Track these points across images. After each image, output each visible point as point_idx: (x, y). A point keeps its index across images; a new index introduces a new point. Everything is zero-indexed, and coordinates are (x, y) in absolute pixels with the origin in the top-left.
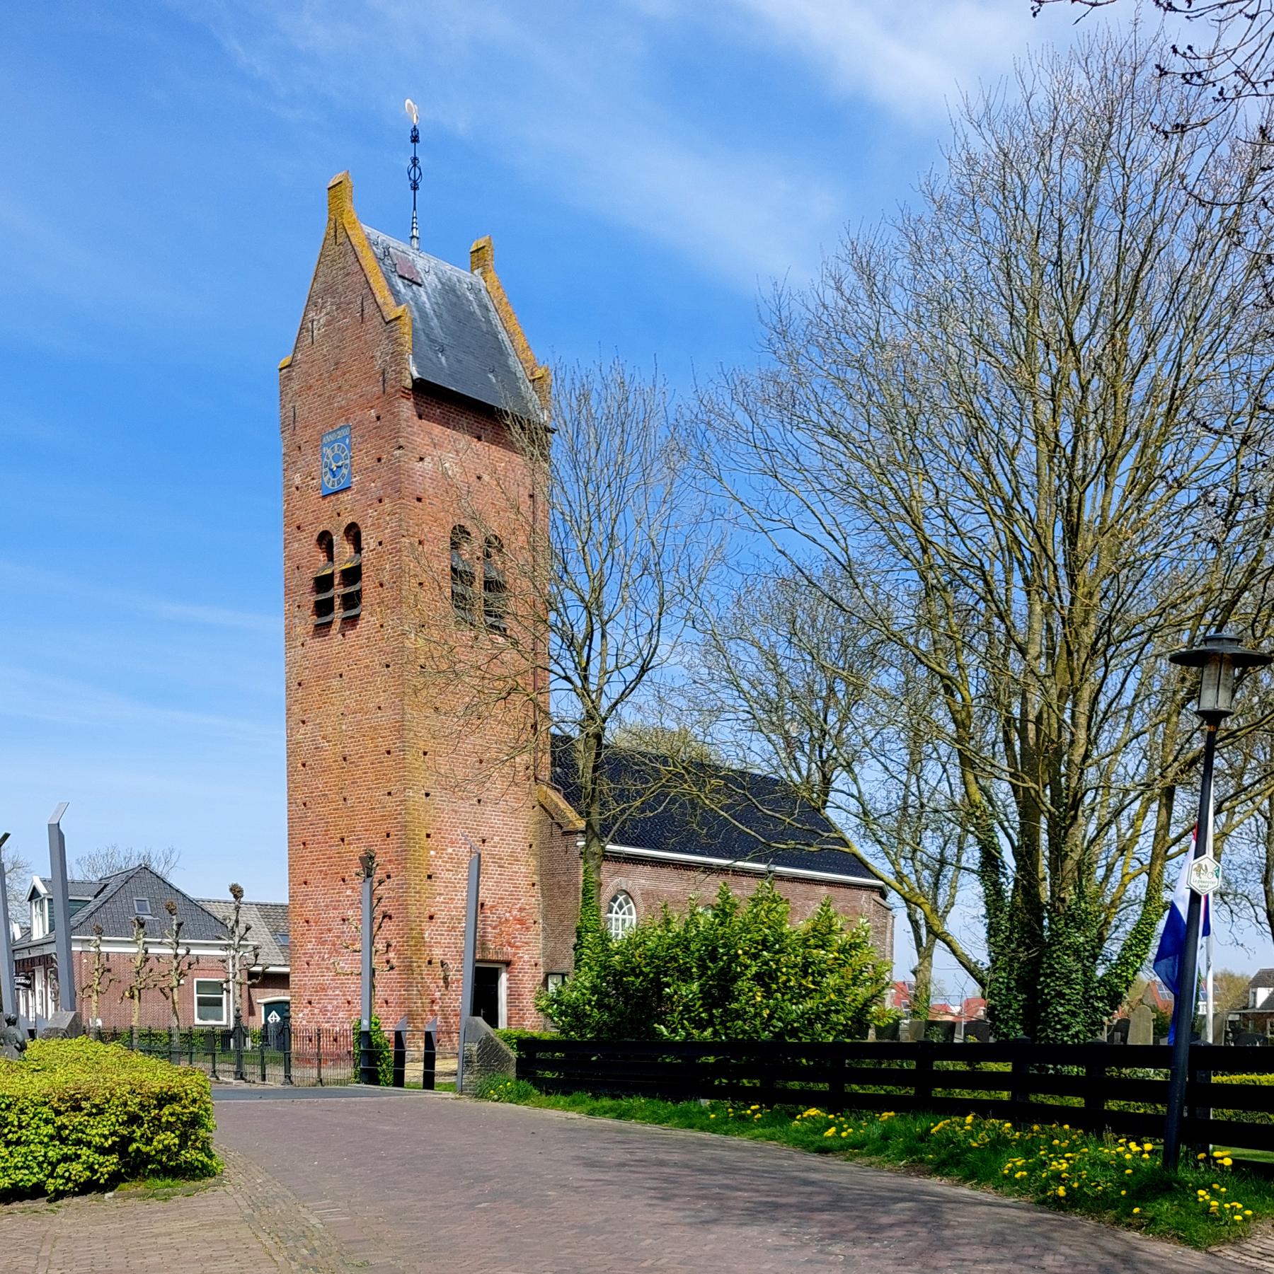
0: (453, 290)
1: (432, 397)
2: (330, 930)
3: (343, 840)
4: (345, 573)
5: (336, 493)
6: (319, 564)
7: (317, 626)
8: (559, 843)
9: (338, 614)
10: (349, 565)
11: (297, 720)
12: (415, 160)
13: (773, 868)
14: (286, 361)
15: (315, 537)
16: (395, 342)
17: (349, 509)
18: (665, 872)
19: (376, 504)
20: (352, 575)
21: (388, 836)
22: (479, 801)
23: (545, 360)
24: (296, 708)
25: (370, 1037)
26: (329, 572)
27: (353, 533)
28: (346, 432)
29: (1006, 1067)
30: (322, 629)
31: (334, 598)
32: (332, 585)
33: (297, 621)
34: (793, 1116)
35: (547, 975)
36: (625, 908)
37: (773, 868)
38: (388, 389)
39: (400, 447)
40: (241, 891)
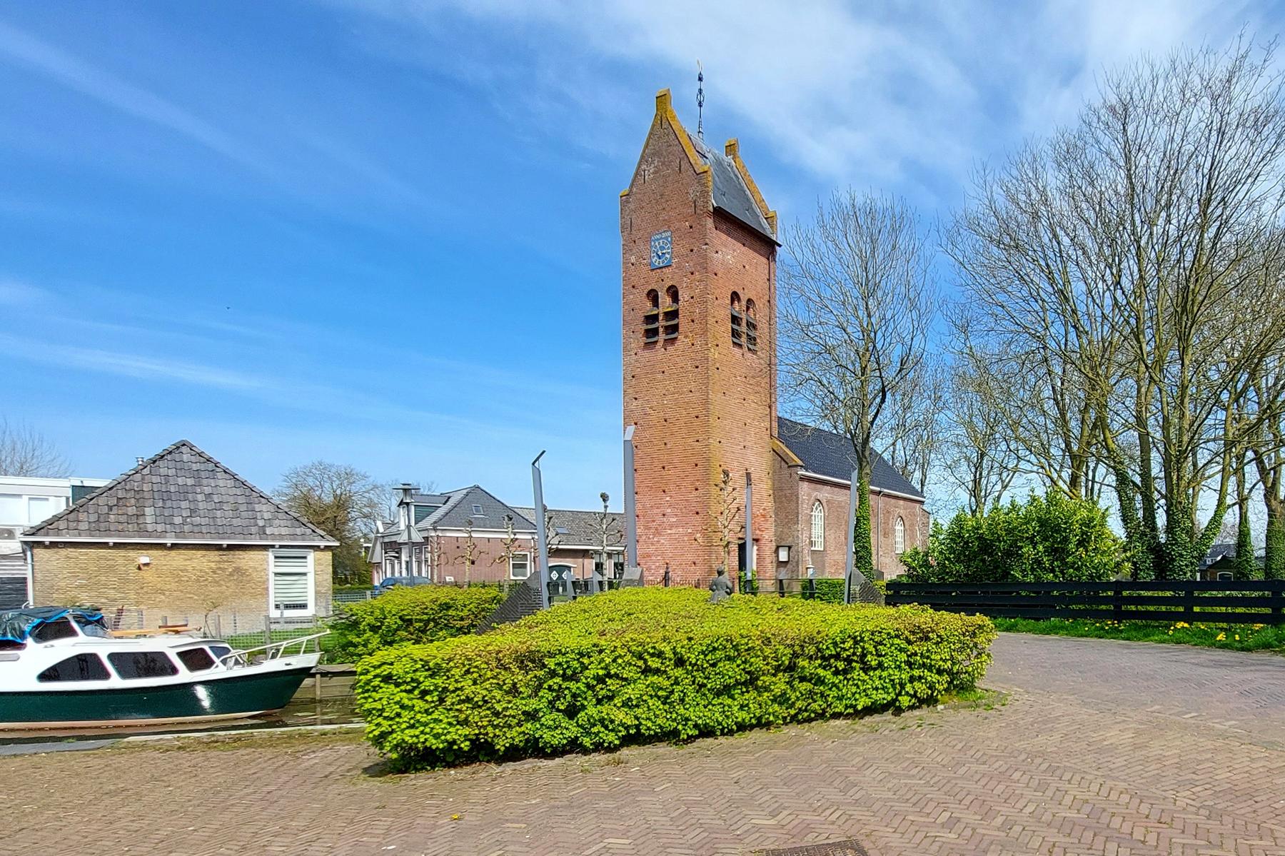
4: (666, 314)
6: (648, 308)
8: (786, 472)
9: (662, 336)
11: (631, 396)
12: (700, 91)
14: (626, 190)
20: (673, 315)
23: (778, 207)
24: (630, 391)
27: (674, 293)
31: (660, 325)
34: (1168, 628)
35: (778, 547)
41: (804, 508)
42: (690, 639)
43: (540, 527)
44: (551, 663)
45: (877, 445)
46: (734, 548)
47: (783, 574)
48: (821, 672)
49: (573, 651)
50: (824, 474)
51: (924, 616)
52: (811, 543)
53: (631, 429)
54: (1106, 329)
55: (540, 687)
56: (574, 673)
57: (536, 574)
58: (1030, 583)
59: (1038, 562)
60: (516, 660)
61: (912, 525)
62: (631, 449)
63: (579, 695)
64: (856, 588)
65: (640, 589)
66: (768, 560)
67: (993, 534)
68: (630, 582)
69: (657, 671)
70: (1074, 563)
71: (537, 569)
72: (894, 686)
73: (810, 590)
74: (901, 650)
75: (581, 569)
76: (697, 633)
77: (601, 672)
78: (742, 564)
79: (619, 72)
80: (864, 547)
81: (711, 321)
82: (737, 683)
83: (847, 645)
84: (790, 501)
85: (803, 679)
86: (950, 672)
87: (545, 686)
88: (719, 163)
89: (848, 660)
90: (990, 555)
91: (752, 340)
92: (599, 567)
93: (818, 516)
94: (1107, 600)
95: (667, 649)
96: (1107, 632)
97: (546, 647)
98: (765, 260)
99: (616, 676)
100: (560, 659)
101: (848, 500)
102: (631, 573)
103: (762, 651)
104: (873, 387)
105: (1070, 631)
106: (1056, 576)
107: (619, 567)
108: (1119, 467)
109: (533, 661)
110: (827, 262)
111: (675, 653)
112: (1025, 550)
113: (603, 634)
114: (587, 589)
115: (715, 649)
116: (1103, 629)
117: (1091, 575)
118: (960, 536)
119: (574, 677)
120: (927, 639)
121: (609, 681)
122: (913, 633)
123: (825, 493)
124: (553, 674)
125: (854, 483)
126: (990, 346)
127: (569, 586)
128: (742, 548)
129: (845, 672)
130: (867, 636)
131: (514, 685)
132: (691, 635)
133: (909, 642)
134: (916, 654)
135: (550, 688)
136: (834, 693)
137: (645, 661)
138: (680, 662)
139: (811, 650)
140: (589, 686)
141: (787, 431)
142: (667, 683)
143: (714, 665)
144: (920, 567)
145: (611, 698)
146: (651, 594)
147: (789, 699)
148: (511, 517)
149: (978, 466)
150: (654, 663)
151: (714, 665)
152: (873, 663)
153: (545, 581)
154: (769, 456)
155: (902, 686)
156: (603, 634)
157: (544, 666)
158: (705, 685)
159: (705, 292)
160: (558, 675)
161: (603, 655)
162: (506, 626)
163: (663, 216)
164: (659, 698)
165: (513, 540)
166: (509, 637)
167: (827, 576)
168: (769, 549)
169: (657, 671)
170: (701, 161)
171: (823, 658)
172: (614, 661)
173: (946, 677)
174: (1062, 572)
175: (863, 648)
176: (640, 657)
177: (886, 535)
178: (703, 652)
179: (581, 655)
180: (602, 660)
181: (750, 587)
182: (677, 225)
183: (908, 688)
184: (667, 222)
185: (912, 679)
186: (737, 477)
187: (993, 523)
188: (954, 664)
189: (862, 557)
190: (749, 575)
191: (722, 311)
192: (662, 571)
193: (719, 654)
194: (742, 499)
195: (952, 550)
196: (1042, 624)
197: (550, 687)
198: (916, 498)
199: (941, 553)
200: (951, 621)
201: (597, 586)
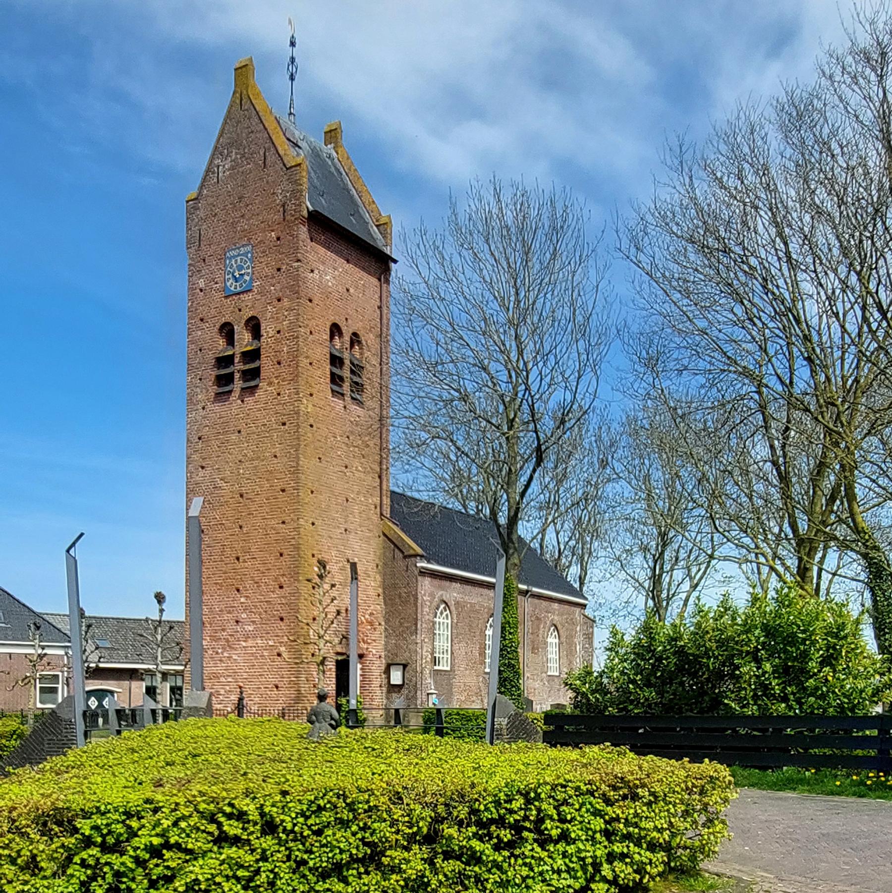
0: (319, 156)
1: (323, 226)
2: (223, 630)
3: (238, 559)
5: (239, 294)
7: (216, 394)
8: (401, 564)
9: (238, 384)
10: (249, 348)
11: (196, 464)
12: (293, 60)
13: (530, 588)
14: (193, 194)
15: (243, 321)
16: (297, 183)
17: (250, 306)
18: (468, 588)
19: (275, 302)
20: (253, 355)
21: (281, 555)
22: (346, 530)
24: (195, 457)
25: (357, 713)
26: (230, 353)
27: (254, 326)
28: (249, 248)
29: (875, 733)
30: (222, 397)
31: (236, 370)
32: (233, 363)
33: (198, 390)
36: (445, 614)
37: (530, 588)
38: (288, 218)
39: (299, 261)
40: (164, 598)
41: (425, 611)
42: (284, 793)
43: (75, 639)
44: (85, 826)
45: (526, 530)
46: (331, 666)
47: (398, 702)
48: (476, 845)
49: (116, 810)
50: (452, 566)
51: (627, 763)
52: (435, 661)
53: (198, 502)
54: (849, 358)
55: (69, 860)
56: (118, 842)
57: (69, 700)
58: (752, 717)
59: (765, 688)
60: (36, 821)
61: (570, 637)
62: (196, 530)
63: (123, 874)
64: (502, 722)
65: (208, 721)
66: (376, 683)
67: (698, 647)
68: (195, 711)
69: (236, 841)
70: (817, 688)
71: (72, 692)
72: (584, 868)
73: (437, 723)
74: (597, 813)
75: (128, 695)
76: (295, 784)
77: (156, 841)
78: (343, 687)
79: (190, 60)
80: (510, 665)
81: (304, 362)
82: (353, 859)
83: (515, 805)
84: (405, 602)
85: (448, 855)
86: (667, 848)
87: (77, 859)
88: (315, 154)
89: (517, 828)
90: (694, 675)
91: (358, 387)
92: (151, 692)
93: (444, 622)
94: (866, 742)
95: (250, 808)
96: (870, 788)
97: (77, 802)
98: (374, 281)
99: (178, 846)
100: (99, 821)
101: (492, 600)
102: (191, 698)
103: (389, 811)
104: (526, 443)
105: (813, 786)
106: (790, 708)
107: (176, 691)
108: (873, 553)
109: (59, 823)
110: (461, 278)
111: (262, 815)
112: (744, 669)
113: (159, 784)
114: (134, 721)
115: (320, 809)
116: (862, 783)
117: (841, 706)
118: (650, 649)
119: (117, 848)
120: (635, 797)
121: (167, 854)
122: (615, 788)
123: (454, 593)
124: (88, 842)
125: (496, 579)
126: (685, 387)
127: (112, 716)
128: (343, 667)
129: (511, 845)
130: (544, 791)
131: (34, 857)
132: (286, 787)
133: (608, 802)
134: (617, 819)
135: (83, 864)
136: (494, 877)
137: (220, 825)
138: (270, 827)
139: (462, 812)
140: (138, 861)
141: (402, 509)
142: (249, 858)
143: (319, 833)
144: (593, 692)
145: (169, 880)
146: (222, 728)
147: (428, 884)
148: (39, 625)
149: (659, 558)
150: (232, 828)
151: (319, 833)
152: (555, 833)
153: (80, 708)
154: (377, 543)
155: (597, 866)
156: (159, 784)
157: (76, 830)
158: (304, 862)
159: (294, 325)
160: (94, 844)
161: (159, 815)
162: (26, 772)
163: (243, 224)
164: (238, 879)
165: (41, 657)
166: (28, 787)
167: (455, 705)
168: (377, 668)
169: (236, 841)
170: (292, 152)
171: (480, 824)
172: (175, 824)
173: (661, 856)
174: (799, 702)
175: (539, 810)
176: (212, 819)
177: (534, 650)
178: (303, 814)
179: (128, 815)
180: (158, 824)
181: (354, 719)
182: (260, 236)
183: (606, 870)
184: (247, 234)
185: (611, 857)
186: (337, 572)
187: (700, 632)
188: (673, 835)
189: (509, 678)
190: (353, 702)
191: (318, 350)
192: (234, 698)
193: (326, 817)
194: (345, 601)
195: (638, 669)
196: (771, 775)
197: (83, 861)
198: (573, 596)
199: (623, 673)
200: (666, 772)
201: (148, 716)
